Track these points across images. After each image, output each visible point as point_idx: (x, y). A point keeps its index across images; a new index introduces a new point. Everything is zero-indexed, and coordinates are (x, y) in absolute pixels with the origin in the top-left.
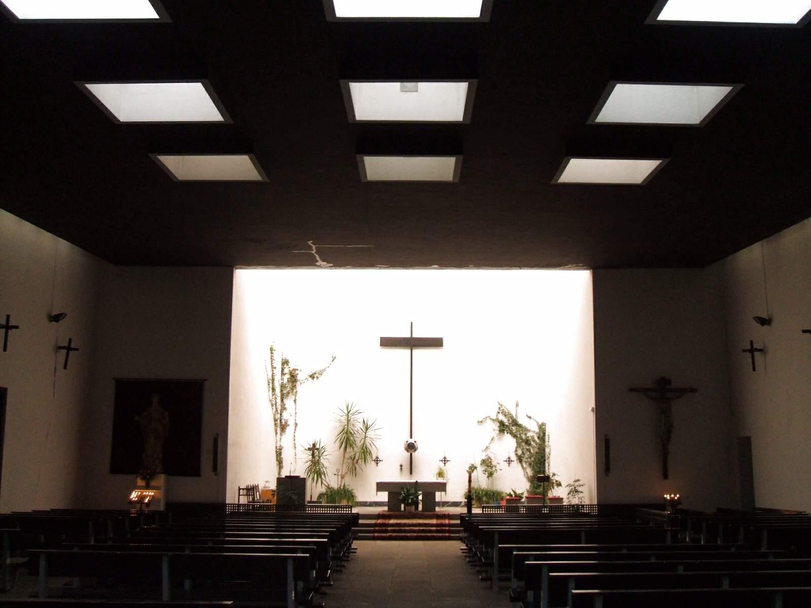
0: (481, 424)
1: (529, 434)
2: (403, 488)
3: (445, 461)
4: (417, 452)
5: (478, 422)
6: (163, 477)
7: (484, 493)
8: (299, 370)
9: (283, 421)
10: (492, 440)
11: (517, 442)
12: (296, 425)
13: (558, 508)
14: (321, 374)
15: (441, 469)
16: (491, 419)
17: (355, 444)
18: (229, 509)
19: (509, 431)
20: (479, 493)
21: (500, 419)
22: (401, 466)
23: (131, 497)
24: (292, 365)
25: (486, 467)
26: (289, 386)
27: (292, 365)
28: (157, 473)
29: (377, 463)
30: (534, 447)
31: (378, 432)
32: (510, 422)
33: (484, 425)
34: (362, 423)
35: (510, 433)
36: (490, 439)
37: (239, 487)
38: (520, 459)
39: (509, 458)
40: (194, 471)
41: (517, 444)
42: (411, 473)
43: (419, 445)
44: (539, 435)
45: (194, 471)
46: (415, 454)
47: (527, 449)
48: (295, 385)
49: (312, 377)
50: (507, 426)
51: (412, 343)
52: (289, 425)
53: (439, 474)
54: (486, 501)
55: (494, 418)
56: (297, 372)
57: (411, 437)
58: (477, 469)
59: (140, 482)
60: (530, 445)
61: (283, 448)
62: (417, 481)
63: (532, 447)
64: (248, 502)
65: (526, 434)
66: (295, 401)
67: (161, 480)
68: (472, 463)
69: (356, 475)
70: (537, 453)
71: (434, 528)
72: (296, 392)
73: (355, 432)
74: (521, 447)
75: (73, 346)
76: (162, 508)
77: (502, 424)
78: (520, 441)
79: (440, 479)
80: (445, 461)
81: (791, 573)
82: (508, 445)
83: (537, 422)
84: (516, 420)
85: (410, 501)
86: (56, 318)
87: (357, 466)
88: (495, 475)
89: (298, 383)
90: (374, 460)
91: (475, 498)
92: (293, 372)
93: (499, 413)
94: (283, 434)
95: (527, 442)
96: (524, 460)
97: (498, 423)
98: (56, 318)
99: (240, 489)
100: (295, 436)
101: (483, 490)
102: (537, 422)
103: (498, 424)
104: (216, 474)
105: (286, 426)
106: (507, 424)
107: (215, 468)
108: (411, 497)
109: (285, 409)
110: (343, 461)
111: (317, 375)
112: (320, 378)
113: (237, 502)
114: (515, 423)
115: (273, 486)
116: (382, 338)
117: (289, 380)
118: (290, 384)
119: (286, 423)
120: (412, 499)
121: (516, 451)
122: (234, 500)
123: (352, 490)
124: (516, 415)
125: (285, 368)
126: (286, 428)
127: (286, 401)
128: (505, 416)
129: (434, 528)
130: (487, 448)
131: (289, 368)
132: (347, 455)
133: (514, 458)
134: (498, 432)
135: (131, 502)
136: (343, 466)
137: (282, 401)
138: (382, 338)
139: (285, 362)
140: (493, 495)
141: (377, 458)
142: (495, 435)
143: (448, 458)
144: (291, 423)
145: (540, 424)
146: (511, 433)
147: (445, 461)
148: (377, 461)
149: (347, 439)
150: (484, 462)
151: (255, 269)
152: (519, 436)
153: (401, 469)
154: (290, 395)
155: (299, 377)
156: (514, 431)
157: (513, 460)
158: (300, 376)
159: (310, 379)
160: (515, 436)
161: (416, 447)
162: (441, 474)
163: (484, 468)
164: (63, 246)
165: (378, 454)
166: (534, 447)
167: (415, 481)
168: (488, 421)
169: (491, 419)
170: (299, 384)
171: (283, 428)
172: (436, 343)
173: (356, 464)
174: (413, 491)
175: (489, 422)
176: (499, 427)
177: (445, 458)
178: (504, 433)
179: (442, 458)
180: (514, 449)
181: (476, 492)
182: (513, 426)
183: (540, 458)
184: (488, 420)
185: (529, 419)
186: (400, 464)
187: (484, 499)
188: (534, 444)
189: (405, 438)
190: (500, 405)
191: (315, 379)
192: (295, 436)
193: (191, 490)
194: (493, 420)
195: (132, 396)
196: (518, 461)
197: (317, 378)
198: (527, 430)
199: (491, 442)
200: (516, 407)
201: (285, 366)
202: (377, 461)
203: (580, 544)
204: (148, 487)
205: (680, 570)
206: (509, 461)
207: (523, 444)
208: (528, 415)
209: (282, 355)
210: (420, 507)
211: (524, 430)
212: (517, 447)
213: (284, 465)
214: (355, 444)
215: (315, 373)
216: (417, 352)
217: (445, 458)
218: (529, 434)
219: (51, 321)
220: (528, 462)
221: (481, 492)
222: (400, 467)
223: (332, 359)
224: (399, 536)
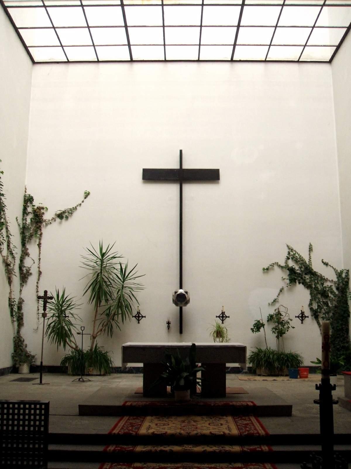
0: (267, 272)
1: (326, 284)
2: (168, 357)
3: (223, 316)
4: (188, 305)
5: (264, 269)
7: (275, 357)
8: (45, 209)
9: (24, 269)
10: (281, 291)
11: (311, 294)
12: (40, 273)
14: (71, 213)
15: (219, 327)
16: (280, 266)
17: (111, 297)
19: (301, 281)
20: (269, 357)
22: (169, 323)
24: (37, 203)
25: (277, 324)
27: (37, 203)
29: (139, 320)
30: (332, 301)
31: (137, 281)
32: (303, 269)
33: (271, 272)
34: (119, 270)
35: (303, 284)
36: (279, 291)
38: (315, 314)
39: (302, 313)
41: (312, 296)
42: (181, 332)
43: (192, 297)
44: (338, 285)
46: (185, 309)
47: (323, 302)
48: (40, 227)
53: (217, 333)
54: (278, 367)
55: (283, 264)
57: (181, 287)
58: (265, 326)
60: (327, 297)
61: (23, 301)
62: (194, 345)
63: (330, 300)
65: (323, 284)
66: (39, 245)
69: (111, 336)
70: (336, 307)
71: (237, 449)
73: (112, 281)
74: (317, 300)
77: (292, 271)
78: (315, 292)
79: (218, 339)
80: (223, 317)
82: (300, 298)
83: (335, 269)
84: (310, 268)
85: (182, 383)
87: (113, 323)
88: (287, 334)
89: (44, 223)
90: (135, 317)
91: (265, 363)
93: (288, 258)
95: (324, 294)
96: (321, 315)
100: (37, 286)
101: (273, 353)
102: (335, 269)
105: (28, 275)
106: (298, 272)
108: (185, 374)
109: (27, 254)
111: (67, 214)
112: (70, 219)
114: (308, 270)
116: (144, 170)
118: (34, 225)
119: (28, 271)
120: (186, 378)
121: (311, 304)
123: (106, 353)
124: (310, 260)
125: (28, 206)
126: (27, 278)
128: (297, 262)
129: (237, 449)
132: (101, 310)
133: (308, 313)
134: (288, 281)
136: (95, 323)
137: (24, 244)
138: (144, 170)
139: (28, 200)
140: (288, 360)
141: (139, 313)
142: (285, 286)
143: (227, 314)
144: (34, 271)
145: (339, 271)
146: (304, 283)
147: (223, 316)
148: (139, 317)
150: (271, 318)
152: (313, 286)
153: (169, 327)
154: (34, 239)
156: (308, 281)
158: (47, 216)
159: (58, 220)
160: (308, 286)
161: (188, 299)
162: (219, 333)
163: (273, 325)
165: (140, 308)
166: (332, 301)
167: (190, 344)
169: (280, 266)
170: (45, 225)
171: (24, 276)
173: (111, 321)
174: (187, 362)
176: (289, 275)
177: (223, 313)
178: (296, 283)
179: (219, 313)
180: (308, 302)
181: (265, 355)
182: (306, 274)
183: (342, 313)
184: (276, 267)
185: (325, 266)
186: (167, 320)
187: (276, 364)
188: (332, 296)
189: (173, 288)
190: (289, 249)
191: (64, 218)
192: (37, 286)
194: (282, 267)
196: (313, 317)
198: (323, 279)
199: (279, 294)
200: (310, 251)
201: (29, 204)
202: (139, 317)
206: (302, 317)
207: (319, 296)
208: (324, 261)
209: (26, 192)
210: (199, 388)
211: (319, 279)
212: (311, 300)
213: (24, 322)
214: (111, 297)
217: (223, 313)
218: (326, 284)
220: (326, 318)
221: (271, 356)
222: (167, 325)
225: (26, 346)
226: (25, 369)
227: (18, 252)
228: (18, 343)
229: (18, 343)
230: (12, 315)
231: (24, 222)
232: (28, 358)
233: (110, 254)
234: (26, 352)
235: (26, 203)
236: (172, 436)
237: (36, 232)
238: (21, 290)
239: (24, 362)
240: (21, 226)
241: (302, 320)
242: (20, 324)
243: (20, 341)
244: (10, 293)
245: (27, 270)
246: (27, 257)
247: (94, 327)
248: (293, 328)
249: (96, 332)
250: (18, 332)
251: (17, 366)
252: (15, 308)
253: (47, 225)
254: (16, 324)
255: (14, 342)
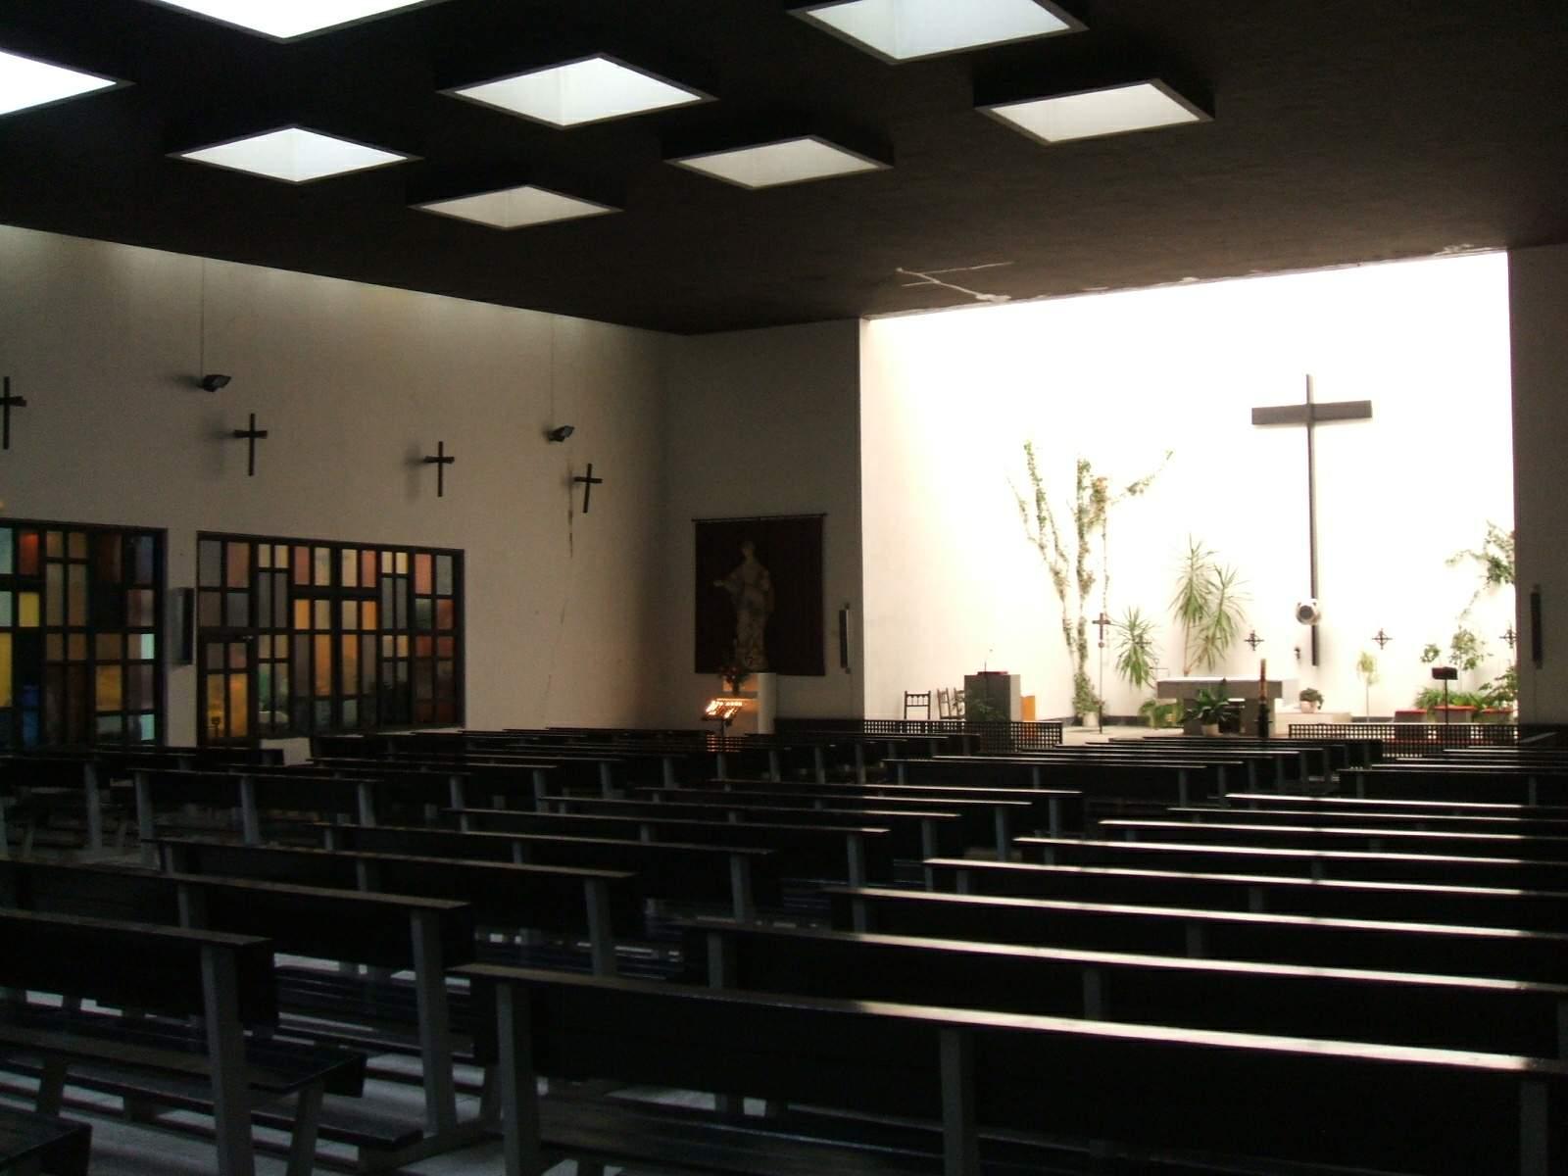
6: (761, 677)
9: (1084, 574)
10: (1475, 596)
12: (1107, 578)
13: (1460, 730)
16: (1473, 555)
18: (1363, 734)
21: (1491, 554)
22: (1298, 650)
23: (708, 710)
26: (1092, 510)
28: (752, 671)
29: (1254, 645)
37: (906, 692)
40: (814, 666)
42: (1315, 661)
45: (814, 666)
49: (1132, 490)
50: (1505, 568)
51: (1311, 415)
52: (1094, 580)
55: (1480, 552)
56: (1105, 483)
59: (728, 688)
64: (941, 718)
67: (760, 682)
68: (1431, 643)
72: (1105, 520)
75: (594, 476)
76: (763, 727)
81: (832, 825)
86: (557, 435)
92: (1098, 483)
93: (1489, 542)
94: (1086, 596)
97: (1487, 563)
98: (557, 435)
99: (907, 695)
103: (1486, 565)
104: (848, 671)
107: (844, 662)
110: (1186, 643)
111: (1141, 486)
113: (902, 719)
115: (961, 686)
117: (1093, 498)
122: (898, 712)
127: (1087, 537)
130: (1465, 612)
131: (1091, 476)
134: (1485, 580)
135: (706, 718)
137: (1081, 535)
143: (1386, 634)
147: (1381, 639)
149: (1192, 607)
151: (971, 307)
153: (1298, 656)
155: (1108, 493)
157: (1503, 640)
159: (1129, 494)
164: (569, 326)
167: (1220, 679)
168: (1468, 558)
169: (1473, 555)
171: (1085, 585)
172: (1359, 411)
175: (1469, 560)
176: (1489, 570)
190: (1490, 525)
193: (810, 698)
195: (718, 543)
197: (1142, 491)
203: (897, 784)
204: (736, 694)
205: (732, 819)
215: (1136, 484)
216: (1320, 430)
217: (1381, 634)
219: (551, 440)
223: (1166, 455)
224: (534, 764)
225: (1093, 688)
226: (1091, 719)
227: (1072, 552)
228: (1081, 684)
229: (1081, 684)
230: (1069, 644)
231: (1080, 501)
232: (1097, 706)
233: (1202, 551)
234: (1093, 697)
235: (1081, 473)
236: (846, 640)
237: (1098, 516)
238: (1081, 606)
239: (1090, 710)
240: (1076, 511)
241: (1382, 644)
242: (1083, 657)
243: (1084, 680)
244: (1064, 612)
245: (1088, 574)
246: (1087, 555)
247: (1186, 658)
248: (1490, 655)
249: (1188, 664)
250: (1081, 667)
251: (1080, 715)
252: (1074, 634)
253: (1113, 504)
254: (1076, 655)
255: (1076, 681)
